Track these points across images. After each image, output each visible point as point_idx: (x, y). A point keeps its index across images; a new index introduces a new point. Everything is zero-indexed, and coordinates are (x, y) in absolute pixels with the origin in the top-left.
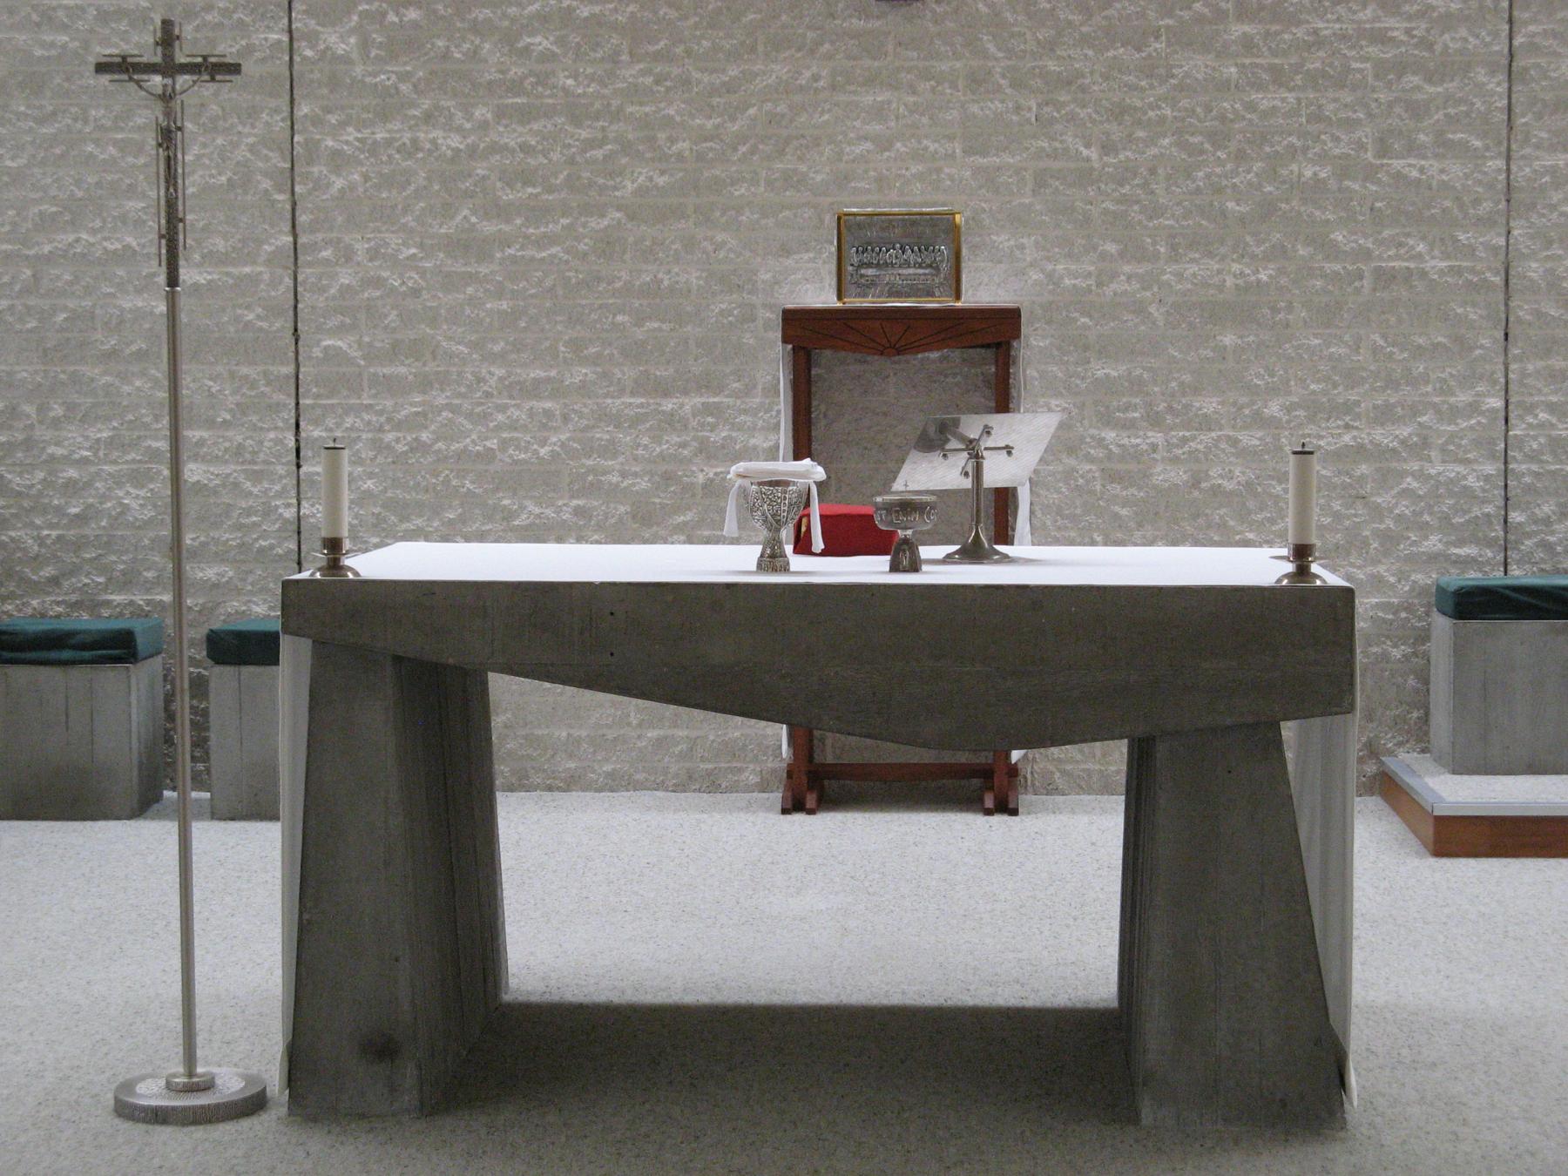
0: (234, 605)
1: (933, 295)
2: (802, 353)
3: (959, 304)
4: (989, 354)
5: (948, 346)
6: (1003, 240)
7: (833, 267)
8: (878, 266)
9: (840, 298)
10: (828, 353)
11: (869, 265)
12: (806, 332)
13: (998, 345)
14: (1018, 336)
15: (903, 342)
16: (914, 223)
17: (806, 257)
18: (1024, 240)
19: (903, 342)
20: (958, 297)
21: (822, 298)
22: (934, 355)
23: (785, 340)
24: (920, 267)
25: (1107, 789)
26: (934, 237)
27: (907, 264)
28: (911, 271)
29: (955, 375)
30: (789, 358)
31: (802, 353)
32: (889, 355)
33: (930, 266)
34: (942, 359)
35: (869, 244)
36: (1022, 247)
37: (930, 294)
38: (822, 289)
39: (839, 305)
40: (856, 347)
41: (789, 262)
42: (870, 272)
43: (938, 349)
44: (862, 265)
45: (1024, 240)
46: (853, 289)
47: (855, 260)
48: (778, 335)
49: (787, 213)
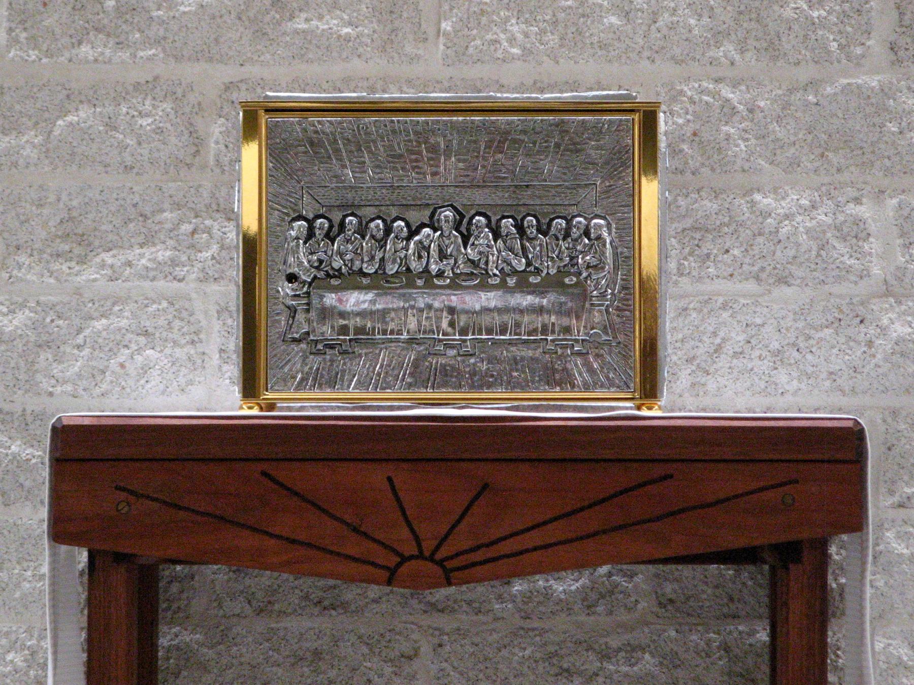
0: (82, 601)
1: (564, 380)
2: (119, 577)
3: (654, 412)
4: (750, 582)
5: (614, 559)
6: (789, 206)
7: (230, 290)
8: (379, 281)
9: (250, 389)
10: (215, 574)
11: (352, 279)
12: (128, 498)
13: (788, 553)
14: (852, 517)
15: (460, 541)
16: (502, 140)
17: (144, 257)
18: (864, 211)
19: (460, 541)
20: (649, 389)
21: (198, 393)
22: (565, 585)
23: (62, 530)
24: (523, 286)
25: (760, 617)
26: (547, 176)
27: (478, 276)
28: (490, 299)
29: (632, 650)
30: (77, 593)
31: (119, 577)
32: (417, 584)
33: (555, 283)
34: (588, 601)
35: (351, 208)
36: (856, 233)
37: (554, 376)
38: (197, 363)
39: (251, 411)
40: (304, 554)
41: (89, 275)
42: (356, 300)
43: (579, 565)
44: (330, 277)
45: (864, 211)
46: (297, 360)
47: (301, 260)
48: (36, 516)
49: (83, 114)
